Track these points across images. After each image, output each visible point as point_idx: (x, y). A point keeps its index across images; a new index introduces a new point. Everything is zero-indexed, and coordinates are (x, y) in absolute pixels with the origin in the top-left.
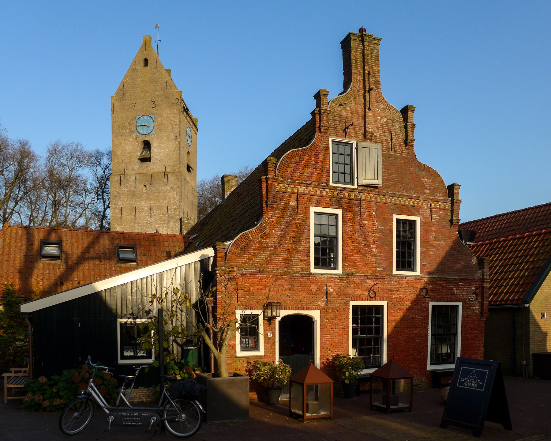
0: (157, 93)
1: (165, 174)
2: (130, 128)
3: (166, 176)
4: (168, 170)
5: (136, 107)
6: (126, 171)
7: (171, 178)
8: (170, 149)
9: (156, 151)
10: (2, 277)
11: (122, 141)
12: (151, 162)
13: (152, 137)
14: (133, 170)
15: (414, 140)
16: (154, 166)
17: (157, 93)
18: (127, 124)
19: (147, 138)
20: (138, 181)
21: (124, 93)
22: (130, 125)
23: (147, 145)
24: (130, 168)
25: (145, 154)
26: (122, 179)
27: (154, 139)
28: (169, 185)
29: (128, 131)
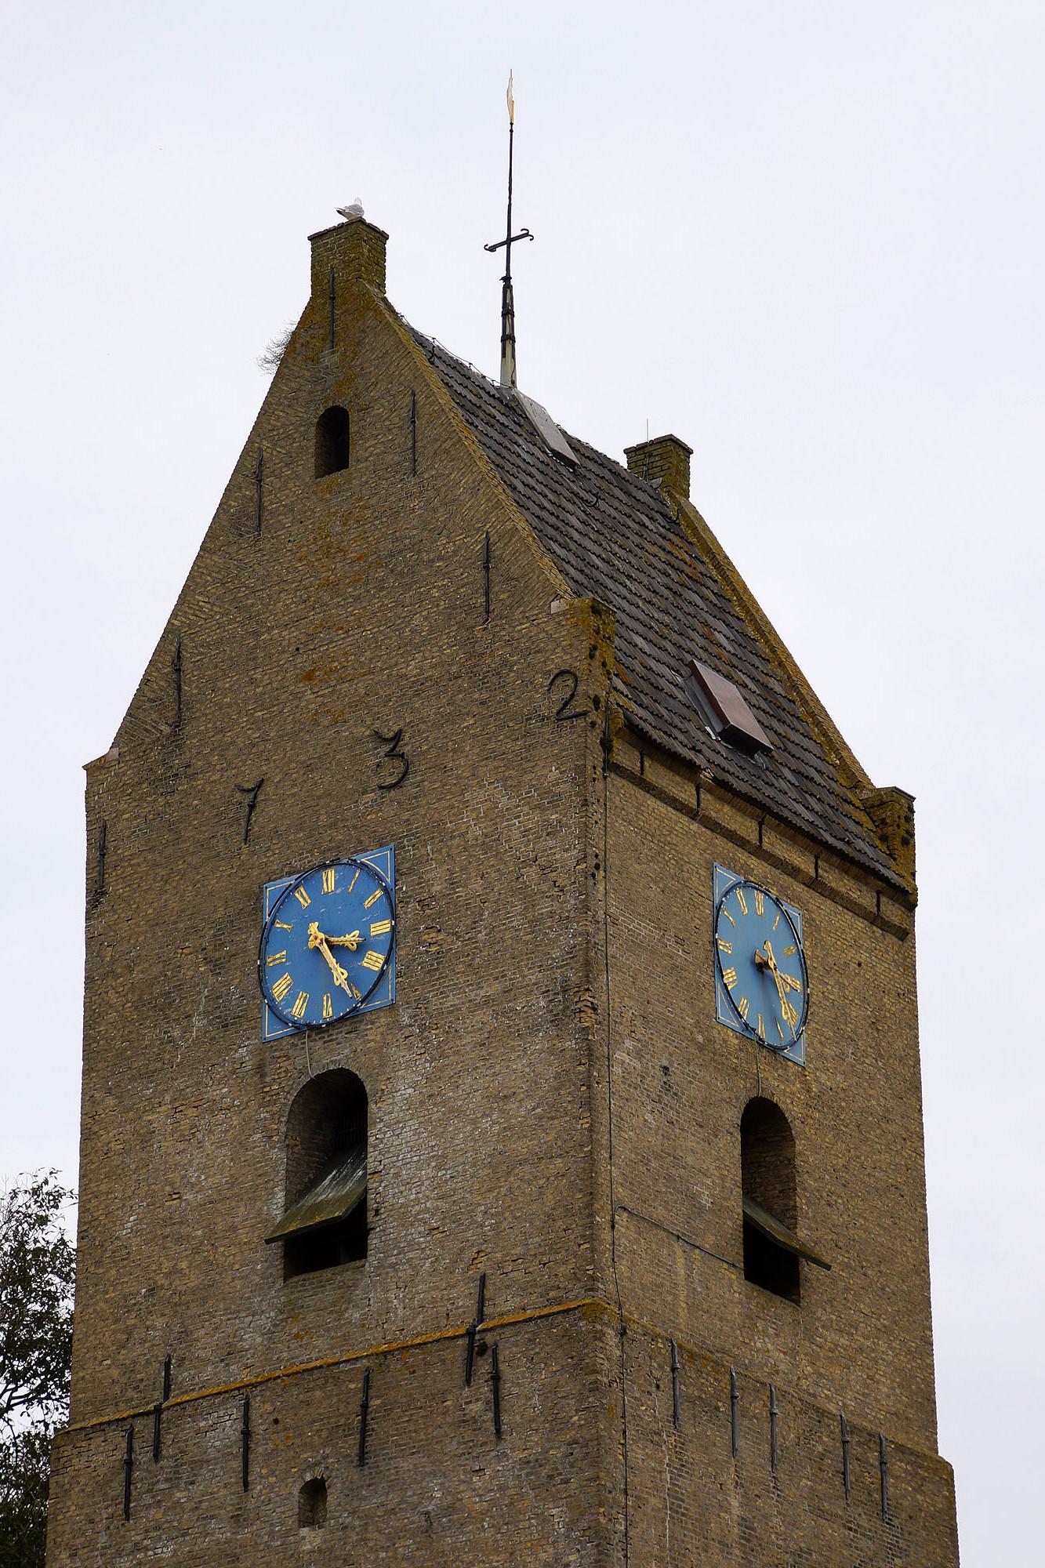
0: (412, 669)
1: (477, 1347)
2: (214, 997)
3: (483, 1366)
4: (505, 1304)
5: (267, 814)
6: (182, 1376)
7: (527, 1381)
8: (519, 1111)
9: (403, 1146)
10: (268, 1564)
11: (158, 1119)
12: (372, 1259)
13: (373, 1034)
14: (230, 1353)
15: (665, 459)
16: (403, 1291)
17: (412, 669)
18: (193, 968)
19: (337, 1055)
20: (259, 1450)
21: (178, 724)
22: (216, 966)
23: (335, 1116)
24: (206, 1343)
25: (331, 1196)
26: (143, 1456)
27: (399, 1054)
28: (511, 1440)
29: (198, 1022)
